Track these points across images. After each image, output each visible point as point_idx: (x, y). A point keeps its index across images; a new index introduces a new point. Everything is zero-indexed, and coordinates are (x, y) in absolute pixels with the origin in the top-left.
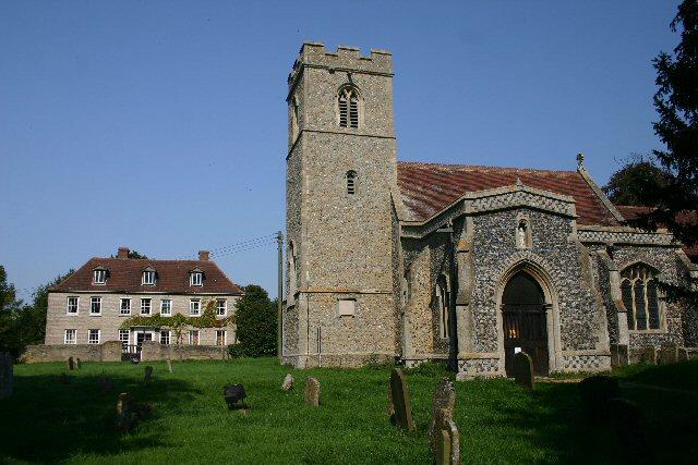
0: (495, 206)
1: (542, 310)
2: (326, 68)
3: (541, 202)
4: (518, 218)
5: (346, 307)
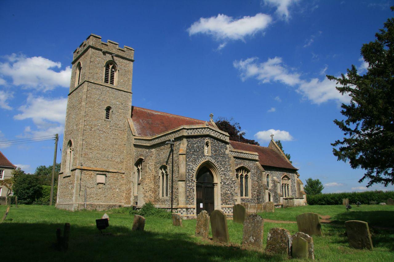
0: (196, 134)
1: (212, 185)
2: (101, 50)
3: (215, 134)
4: (206, 141)
5: (101, 179)
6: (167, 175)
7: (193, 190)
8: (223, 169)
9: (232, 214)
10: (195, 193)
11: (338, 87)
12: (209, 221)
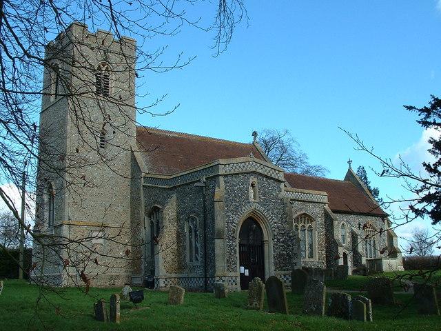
6: (196, 231)
7: (235, 251)
8: (275, 220)
9: (290, 283)
10: (238, 255)
11: (429, 106)
12: (264, 291)
